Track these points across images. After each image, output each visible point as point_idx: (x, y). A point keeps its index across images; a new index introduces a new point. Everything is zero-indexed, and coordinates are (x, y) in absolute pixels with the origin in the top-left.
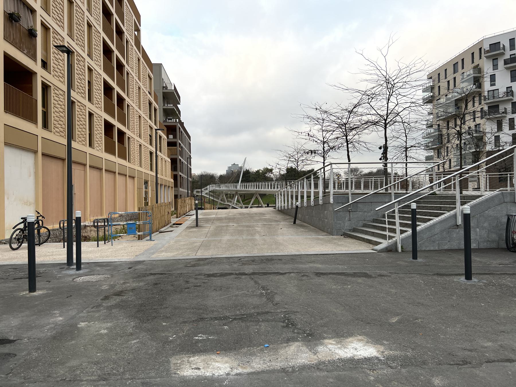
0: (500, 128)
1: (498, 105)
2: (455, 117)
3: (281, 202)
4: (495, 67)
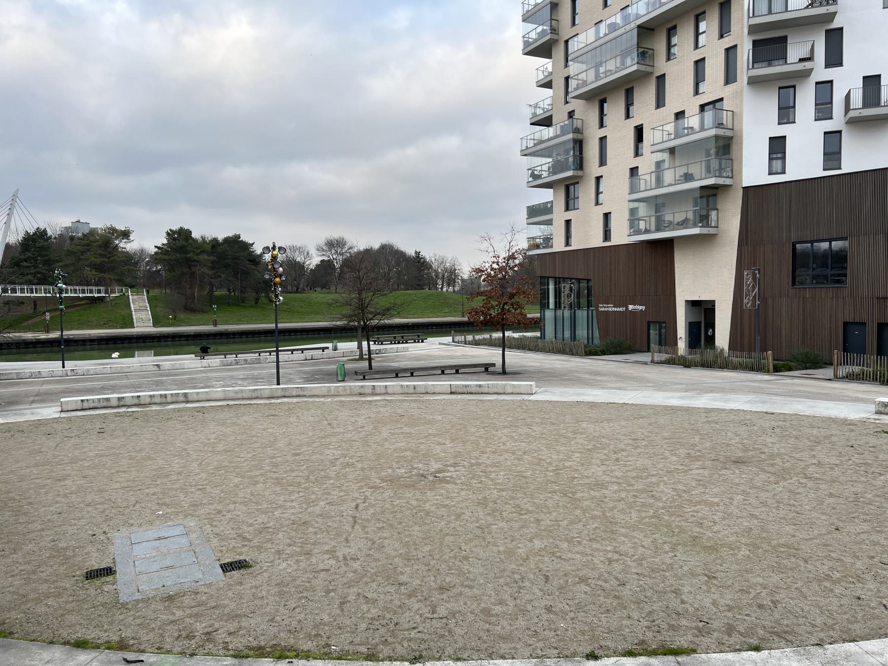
0: (786, 114)
1: (784, 40)
2: (627, 88)
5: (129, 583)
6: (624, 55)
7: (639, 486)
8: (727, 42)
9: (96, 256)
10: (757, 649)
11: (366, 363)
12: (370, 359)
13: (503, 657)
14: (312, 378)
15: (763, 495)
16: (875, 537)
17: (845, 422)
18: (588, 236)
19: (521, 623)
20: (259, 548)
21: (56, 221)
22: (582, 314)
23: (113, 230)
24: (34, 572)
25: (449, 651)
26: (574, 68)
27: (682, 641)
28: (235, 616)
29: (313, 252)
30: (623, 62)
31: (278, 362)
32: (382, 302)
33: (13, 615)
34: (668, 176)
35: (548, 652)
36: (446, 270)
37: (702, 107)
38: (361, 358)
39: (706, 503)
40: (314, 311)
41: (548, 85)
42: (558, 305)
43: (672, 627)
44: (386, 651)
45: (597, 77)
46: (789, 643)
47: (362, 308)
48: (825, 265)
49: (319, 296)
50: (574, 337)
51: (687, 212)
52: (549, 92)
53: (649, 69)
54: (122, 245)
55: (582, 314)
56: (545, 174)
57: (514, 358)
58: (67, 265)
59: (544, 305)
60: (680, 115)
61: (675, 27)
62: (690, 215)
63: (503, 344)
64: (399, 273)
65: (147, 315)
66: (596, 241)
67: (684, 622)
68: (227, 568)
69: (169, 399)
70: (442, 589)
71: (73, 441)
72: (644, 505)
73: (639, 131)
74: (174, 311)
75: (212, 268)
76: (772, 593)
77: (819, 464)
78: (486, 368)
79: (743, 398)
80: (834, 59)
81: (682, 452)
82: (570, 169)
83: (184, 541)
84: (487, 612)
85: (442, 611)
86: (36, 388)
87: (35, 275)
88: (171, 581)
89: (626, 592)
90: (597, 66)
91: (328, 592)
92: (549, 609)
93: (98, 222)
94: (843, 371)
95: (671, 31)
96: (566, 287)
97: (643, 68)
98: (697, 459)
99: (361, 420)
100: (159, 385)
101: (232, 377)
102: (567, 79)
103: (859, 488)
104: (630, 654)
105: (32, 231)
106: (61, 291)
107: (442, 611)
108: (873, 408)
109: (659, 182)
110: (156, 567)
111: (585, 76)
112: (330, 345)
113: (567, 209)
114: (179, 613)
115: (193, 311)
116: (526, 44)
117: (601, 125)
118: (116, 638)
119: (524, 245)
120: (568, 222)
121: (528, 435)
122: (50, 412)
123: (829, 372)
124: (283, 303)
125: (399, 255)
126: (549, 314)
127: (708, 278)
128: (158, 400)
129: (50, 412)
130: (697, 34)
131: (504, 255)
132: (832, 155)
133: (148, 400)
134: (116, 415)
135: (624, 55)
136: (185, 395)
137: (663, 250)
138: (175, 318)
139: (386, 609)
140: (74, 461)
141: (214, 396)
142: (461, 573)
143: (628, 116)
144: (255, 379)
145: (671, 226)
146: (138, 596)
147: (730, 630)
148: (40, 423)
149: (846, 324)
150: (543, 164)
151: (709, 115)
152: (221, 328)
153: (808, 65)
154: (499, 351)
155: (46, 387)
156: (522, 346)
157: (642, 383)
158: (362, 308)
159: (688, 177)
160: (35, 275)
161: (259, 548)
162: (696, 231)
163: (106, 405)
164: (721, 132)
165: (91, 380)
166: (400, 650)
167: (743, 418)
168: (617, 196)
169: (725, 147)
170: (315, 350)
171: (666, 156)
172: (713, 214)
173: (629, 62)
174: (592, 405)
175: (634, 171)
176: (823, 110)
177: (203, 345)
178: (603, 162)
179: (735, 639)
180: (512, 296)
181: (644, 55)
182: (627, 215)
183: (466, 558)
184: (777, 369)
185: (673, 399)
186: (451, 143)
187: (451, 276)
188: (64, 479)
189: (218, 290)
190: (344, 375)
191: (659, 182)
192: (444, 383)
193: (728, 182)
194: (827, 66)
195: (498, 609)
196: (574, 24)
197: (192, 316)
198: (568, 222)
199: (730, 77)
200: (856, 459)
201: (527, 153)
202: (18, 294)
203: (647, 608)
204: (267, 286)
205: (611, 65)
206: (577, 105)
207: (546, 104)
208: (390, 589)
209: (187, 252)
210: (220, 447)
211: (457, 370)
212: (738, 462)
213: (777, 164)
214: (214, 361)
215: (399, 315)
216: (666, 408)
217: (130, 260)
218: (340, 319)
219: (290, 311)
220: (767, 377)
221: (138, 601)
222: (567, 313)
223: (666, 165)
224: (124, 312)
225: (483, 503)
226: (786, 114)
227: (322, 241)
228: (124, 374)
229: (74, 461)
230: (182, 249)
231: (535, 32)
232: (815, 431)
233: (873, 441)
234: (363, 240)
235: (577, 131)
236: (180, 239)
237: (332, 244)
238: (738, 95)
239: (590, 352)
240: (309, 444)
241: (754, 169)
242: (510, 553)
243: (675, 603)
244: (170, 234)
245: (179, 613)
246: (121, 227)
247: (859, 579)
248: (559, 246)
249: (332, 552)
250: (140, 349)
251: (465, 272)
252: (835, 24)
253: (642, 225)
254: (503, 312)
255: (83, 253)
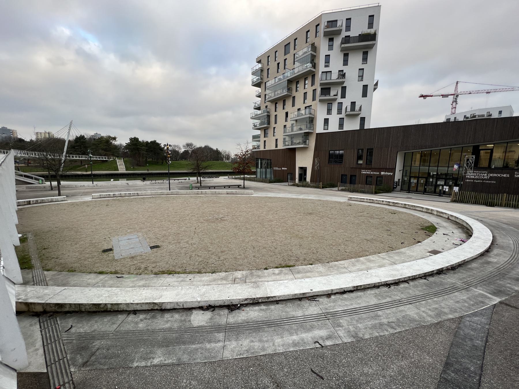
0: (329, 112)
1: (330, 88)
2: (283, 100)
3: (63, 377)
4: (331, 47)
5: (117, 254)
6: (283, 89)
7: (282, 221)
8: (314, 88)
9: (104, 146)
10: (311, 264)
11: (199, 184)
12: (201, 183)
13: (240, 270)
14: (181, 188)
15: (316, 223)
16: (345, 234)
17: (340, 203)
18: (271, 146)
19: (246, 260)
20: (163, 241)
21: (88, 133)
22: (268, 170)
23: (110, 137)
24: (83, 251)
25: (224, 269)
26: (268, 92)
27: (291, 263)
28: (154, 262)
29: (182, 147)
30: (283, 91)
31: (169, 183)
32: (204, 164)
33: (76, 265)
34: (295, 128)
35: (253, 268)
36: (226, 155)
37: (306, 108)
38: (198, 182)
39: (301, 225)
40: (181, 167)
41: (259, 97)
42: (261, 167)
43: (289, 260)
44: (204, 270)
45: (275, 95)
46: (320, 262)
47: (198, 167)
48: (337, 158)
49: (183, 162)
50: (266, 177)
51: (299, 140)
52: (260, 99)
53: (290, 94)
54: (113, 142)
55: (268, 170)
56: (258, 125)
57: (248, 183)
58: (93, 149)
59: (257, 167)
60: (299, 109)
61: (298, 81)
62: (301, 141)
63: (244, 179)
64: (211, 155)
65: (124, 167)
66: (273, 148)
67: (292, 258)
68: (152, 248)
69: (132, 195)
70: (222, 252)
71: (97, 208)
72: (283, 226)
73: (287, 114)
74: (133, 166)
75: (147, 151)
76: (317, 249)
77: (332, 214)
78: (239, 186)
79: (313, 196)
80: (343, 96)
81: (295, 211)
82: (266, 124)
83: (137, 240)
84: (235, 258)
85: (222, 258)
86: (83, 191)
87: (81, 151)
88: (133, 252)
89: (277, 251)
90: (275, 92)
91: (186, 254)
92: (254, 256)
93: (104, 134)
94: (340, 188)
95: (297, 83)
96: (264, 162)
97: (289, 94)
98: (299, 213)
99: (197, 202)
100: (128, 190)
101: (154, 188)
102: (265, 95)
103: (342, 220)
104: (277, 267)
105: (79, 136)
106: (91, 157)
107: (222, 258)
108: (347, 199)
109: (292, 130)
110: (128, 248)
111: (271, 95)
112: (187, 178)
113: (265, 137)
114: (136, 262)
115: (140, 166)
116: (253, 82)
117: (276, 111)
118: (114, 270)
119: (252, 148)
120: (265, 141)
121: (251, 207)
122: (88, 199)
123: (336, 189)
124: (171, 164)
125: (211, 149)
126: (259, 170)
127: (305, 160)
128: (128, 195)
129: (88, 199)
130: (305, 84)
131: (244, 150)
132: (341, 125)
133: (124, 195)
134: (112, 200)
135: (283, 89)
136: (137, 193)
137: (293, 151)
138: (133, 168)
139: (204, 258)
140: (97, 215)
141: (147, 194)
142: (228, 247)
143: (284, 109)
144: (162, 189)
145: (295, 144)
146: (121, 257)
147: (305, 260)
148: (84, 203)
149: (342, 175)
150: (257, 122)
151: (307, 110)
152: (150, 172)
153: (336, 97)
154: (243, 181)
155: (86, 190)
156: (250, 180)
157: (285, 191)
158: (198, 167)
159: (301, 129)
160: (81, 151)
161: (163, 241)
162: (302, 146)
163: (109, 196)
164: (311, 116)
165: (104, 188)
166: (208, 270)
167: (312, 201)
168: (280, 134)
169: (312, 120)
170: (182, 180)
171: (294, 122)
172: (308, 141)
173: (284, 91)
174: (270, 198)
175: (285, 126)
176: (339, 112)
177: (144, 177)
178: (276, 123)
179: (306, 262)
180: (247, 164)
181: (289, 89)
182: (282, 140)
183: (230, 243)
184: (323, 188)
185: (294, 196)
186: (229, 113)
187: (228, 157)
188: (94, 220)
189: (148, 159)
190: (192, 188)
191: (292, 130)
192: (225, 191)
193: (312, 131)
194: (341, 98)
195: (239, 257)
196: (268, 77)
197: (139, 167)
198: (265, 141)
199: (314, 99)
200: (342, 213)
201: (252, 118)
202: (75, 158)
203: (282, 255)
204: (166, 158)
205: (279, 92)
206: (268, 104)
207: (259, 103)
208: (205, 252)
209: (137, 146)
210: (150, 210)
211: (229, 187)
212: (310, 214)
213: (326, 127)
214: (148, 182)
215: (210, 169)
216: (291, 198)
217: (116, 147)
218: (190, 170)
219: (173, 166)
220: (320, 190)
221: (121, 259)
222: (264, 170)
223: (295, 125)
224: (115, 165)
225: (236, 227)
226: (329, 112)
227: (185, 144)
228: (115, 186)
229: (97, 215)
230: (135, 145)
231: (256, 78)
232: (332, 205)
233: (346, 208)
234: (199, 144)
235: (268, 112)
236: (134, 141)
237: (188, 145)
238: (316, 104)
239: (270, 182)
240: (180, 209)
241: (319, 129)
242: (243, 241)
243: (290, 253)
244: (131, 139)
245: (136, 262)
246: (112, 136)
247: (340, 245)
248: (262, 149)
249: (187, 242)
250: (121, 178)
251: (233, 156)
252: (344, 85)
253: (287, 143)
254: (244, 169)
255: (99, 144)
